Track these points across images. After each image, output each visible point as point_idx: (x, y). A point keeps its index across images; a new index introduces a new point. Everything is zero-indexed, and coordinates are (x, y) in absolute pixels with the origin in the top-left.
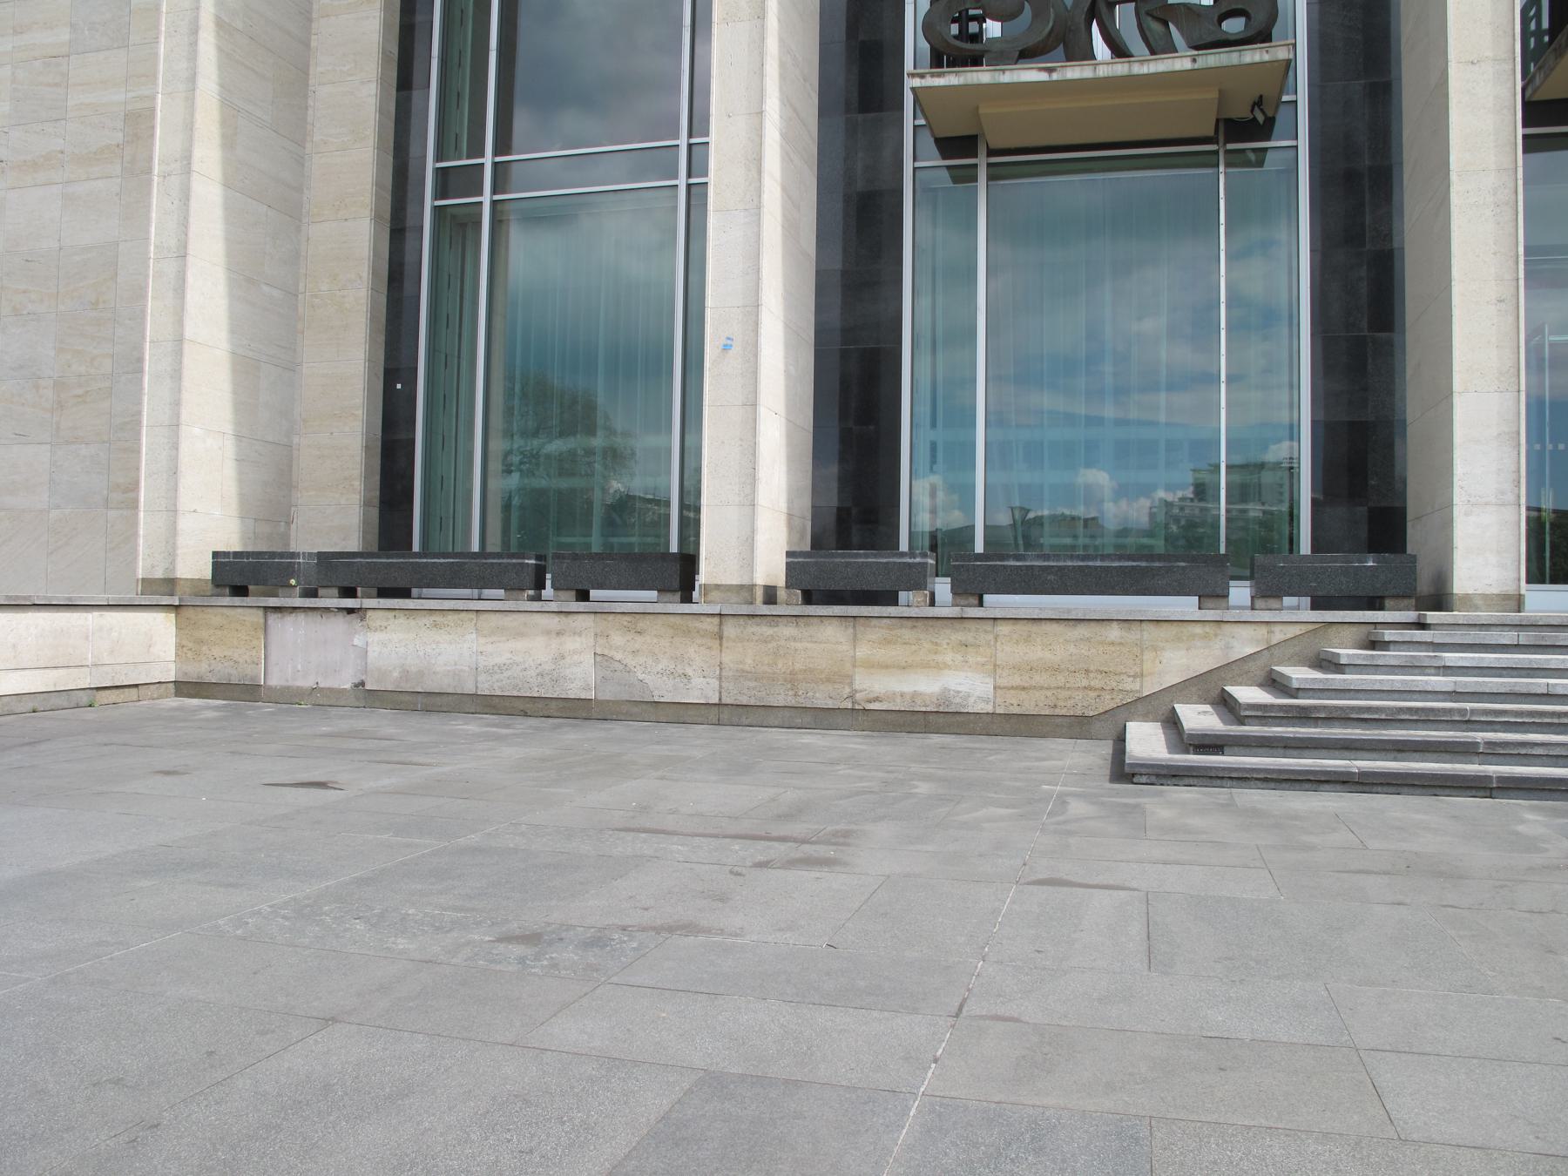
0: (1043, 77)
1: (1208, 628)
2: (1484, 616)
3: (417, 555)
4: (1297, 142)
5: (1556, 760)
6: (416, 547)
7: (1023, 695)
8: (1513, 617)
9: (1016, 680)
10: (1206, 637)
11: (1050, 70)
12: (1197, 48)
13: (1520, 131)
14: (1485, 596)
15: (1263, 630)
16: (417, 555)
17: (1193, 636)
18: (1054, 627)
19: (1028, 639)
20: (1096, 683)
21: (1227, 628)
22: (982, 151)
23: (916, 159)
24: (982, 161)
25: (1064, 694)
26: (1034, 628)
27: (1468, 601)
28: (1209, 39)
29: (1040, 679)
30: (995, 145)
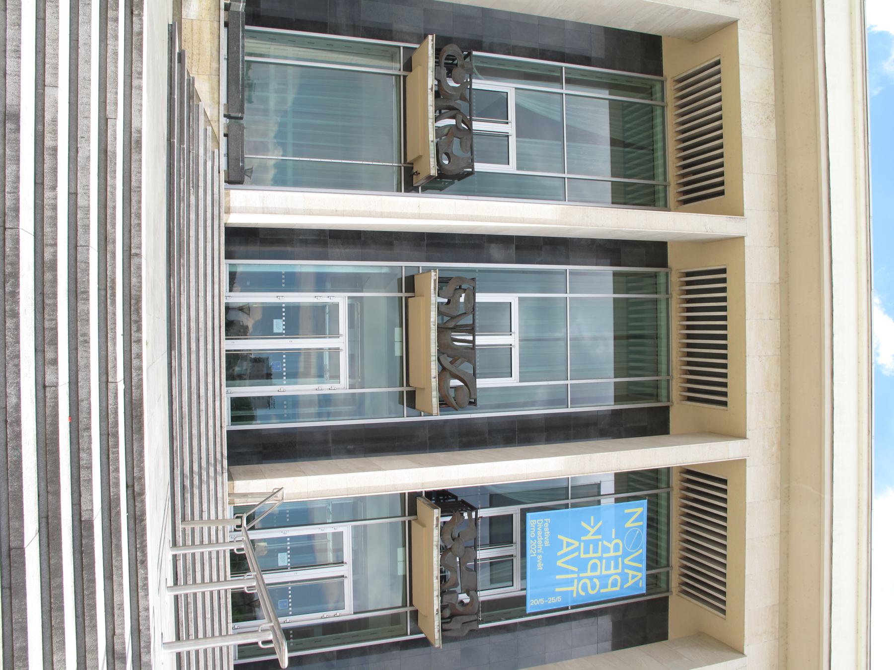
0: (430, 86)
1: (217, 99)
2: (223, 201)
3: (243, 27)
4: (406, 418)
5: (114, 655)
6: (247, 27)
7: (189, 30)
8: (223, 210)
9: (195, 28)
10: (213, 98)
11: (432, 89)
12: (437, 144)
13: (407, 492)
14: (229, 201)
15: (216, 119)
16: (243, 27)
17: (213, 94)
18: (217, 43)
19: (212, 33)
20: (194, 57)
21: (217, 106)
22: (405, 73)
23: (404, 266)
24: (402, 73)
25: (190, 45)
26: (216, 36)
27: (228, 195)
28: (440, 148)
29: (196, 37)
30: (408, 79)
